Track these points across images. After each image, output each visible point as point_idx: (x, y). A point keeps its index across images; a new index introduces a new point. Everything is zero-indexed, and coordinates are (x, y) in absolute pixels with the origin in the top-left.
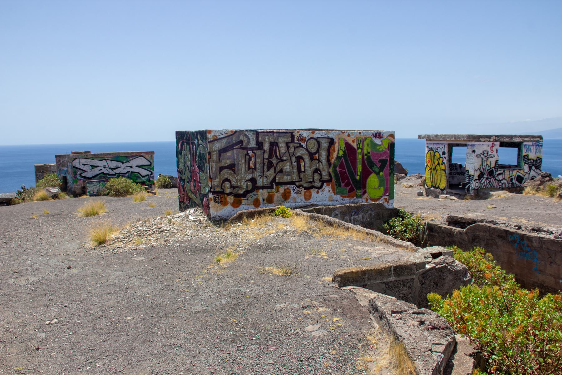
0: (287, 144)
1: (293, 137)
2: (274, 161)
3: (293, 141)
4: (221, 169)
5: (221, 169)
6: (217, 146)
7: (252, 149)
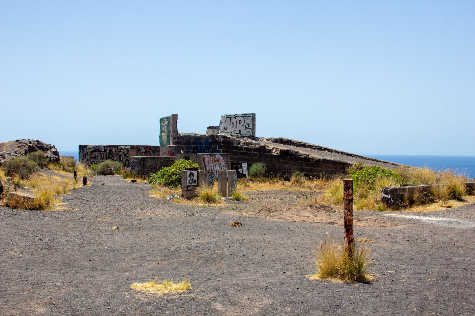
0: (116, 150)
1: (118, 148)
2: (111, 156)
3: (118, 149)
4: (91, 158)
5: (91, 158)
6: (90, 150)
7: (103, 152)
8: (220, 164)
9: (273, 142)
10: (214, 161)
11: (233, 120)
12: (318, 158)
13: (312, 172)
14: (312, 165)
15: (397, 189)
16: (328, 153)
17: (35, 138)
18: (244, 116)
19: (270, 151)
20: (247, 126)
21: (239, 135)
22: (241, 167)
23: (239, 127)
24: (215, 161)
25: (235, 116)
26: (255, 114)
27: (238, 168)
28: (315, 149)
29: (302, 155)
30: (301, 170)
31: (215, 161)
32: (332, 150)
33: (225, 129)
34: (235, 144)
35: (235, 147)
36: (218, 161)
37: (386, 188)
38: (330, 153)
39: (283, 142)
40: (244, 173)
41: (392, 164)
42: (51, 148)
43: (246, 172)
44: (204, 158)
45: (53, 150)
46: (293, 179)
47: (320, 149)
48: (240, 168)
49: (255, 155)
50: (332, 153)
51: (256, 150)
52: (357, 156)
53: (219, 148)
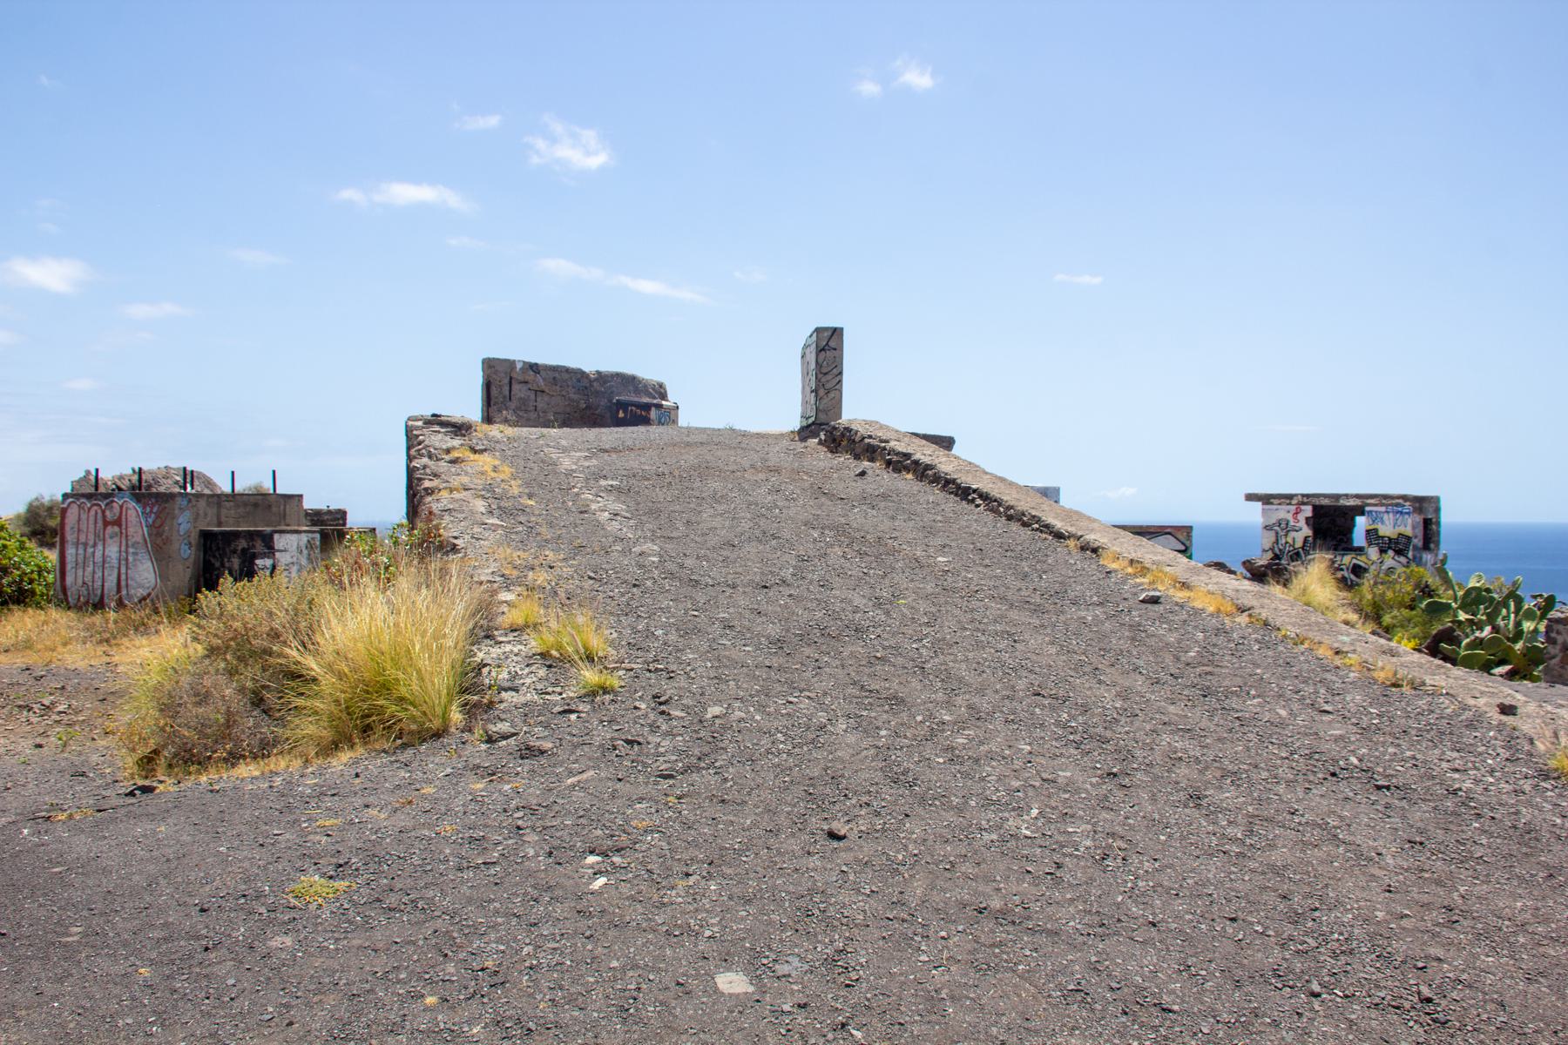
8: (124, 536)
24: (106, 524)
31: (106, 524)
36: (118, 522)
48: (264, 556)
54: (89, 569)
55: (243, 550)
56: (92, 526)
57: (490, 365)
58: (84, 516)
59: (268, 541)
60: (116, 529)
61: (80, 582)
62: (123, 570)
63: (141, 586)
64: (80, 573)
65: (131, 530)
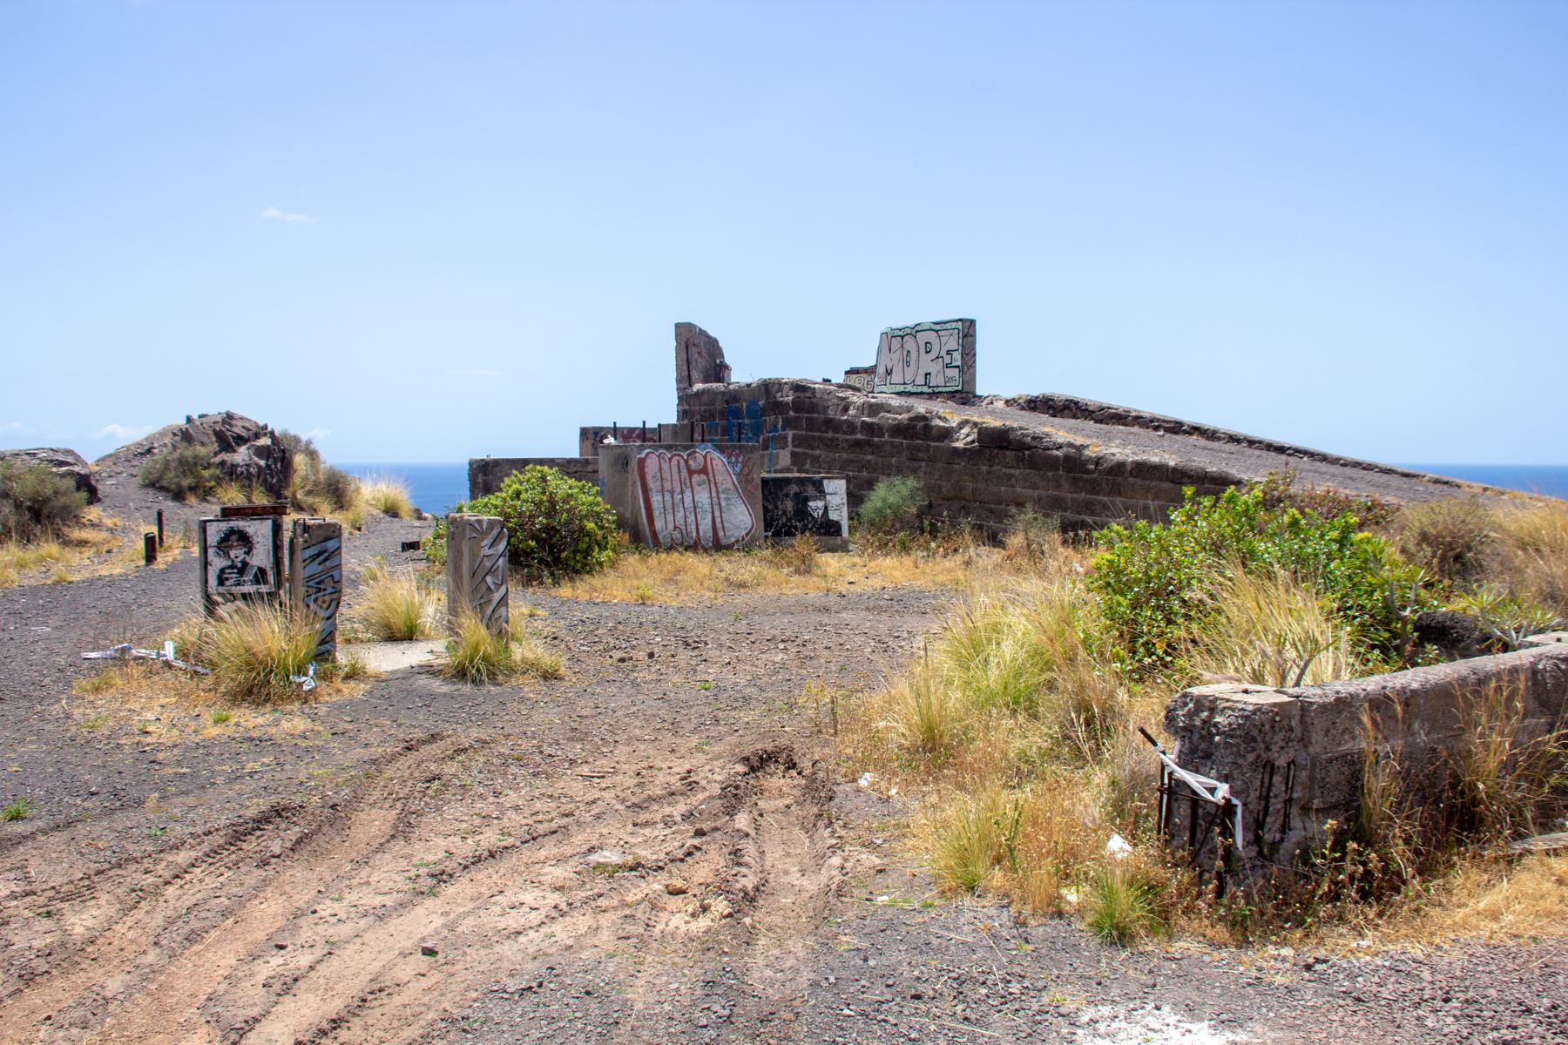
8: (712, 483)
9: (1023, 409)
10: (684, 473)
11: (910, 344)
12: (1119, 457)
13: (1092, 514)
14: (1094, 488)
15: (1304, 707)
16: (1202, 442)
17: (215, 408)
18: (938, 327)
19: (947, 434)
20: (947, 359)
21: (925, 389)
22: (821, 493)
23: (927, 363)
24: (691, 473)
25: (915, 331)
26: (972, 322)
27: (807, 499)
28: (1156, 428)
29: (1060, 447)
30: (1050, 505)
31: (691, 473)
32: (1214, 432)
33: (889, 373)
34: (831, 413)
35: (831, 420)
36: (704, 471)
37: (1200, 702)
38: (1210, 444)
39: (1051, 407)
40: (833, 516)
41: (1437, 481)
42: (257, 436)
43: (840, 514)
44: (642, 462)
45: (265, 441)
46: (1016, 541)
47: (1176, 428)
48: (815, 498)
49: (897, 449)
50: (1216, 445)
51: (898, 430)
52: (1305, 453)
53: (784, 429)
54: (680, 514)
55: (796, 494)
56: (676, 476)
57: (678, 326)
58: (665, 466)
59: (818, 486)
60: (703, 477)
61: (671, 527)
62: (717, 514)
63: (737, 527)
64: (670, 518)
65: (719, 478)
